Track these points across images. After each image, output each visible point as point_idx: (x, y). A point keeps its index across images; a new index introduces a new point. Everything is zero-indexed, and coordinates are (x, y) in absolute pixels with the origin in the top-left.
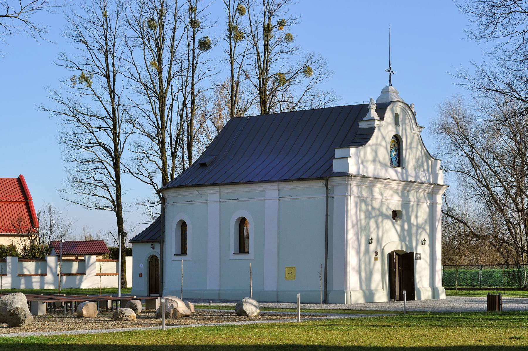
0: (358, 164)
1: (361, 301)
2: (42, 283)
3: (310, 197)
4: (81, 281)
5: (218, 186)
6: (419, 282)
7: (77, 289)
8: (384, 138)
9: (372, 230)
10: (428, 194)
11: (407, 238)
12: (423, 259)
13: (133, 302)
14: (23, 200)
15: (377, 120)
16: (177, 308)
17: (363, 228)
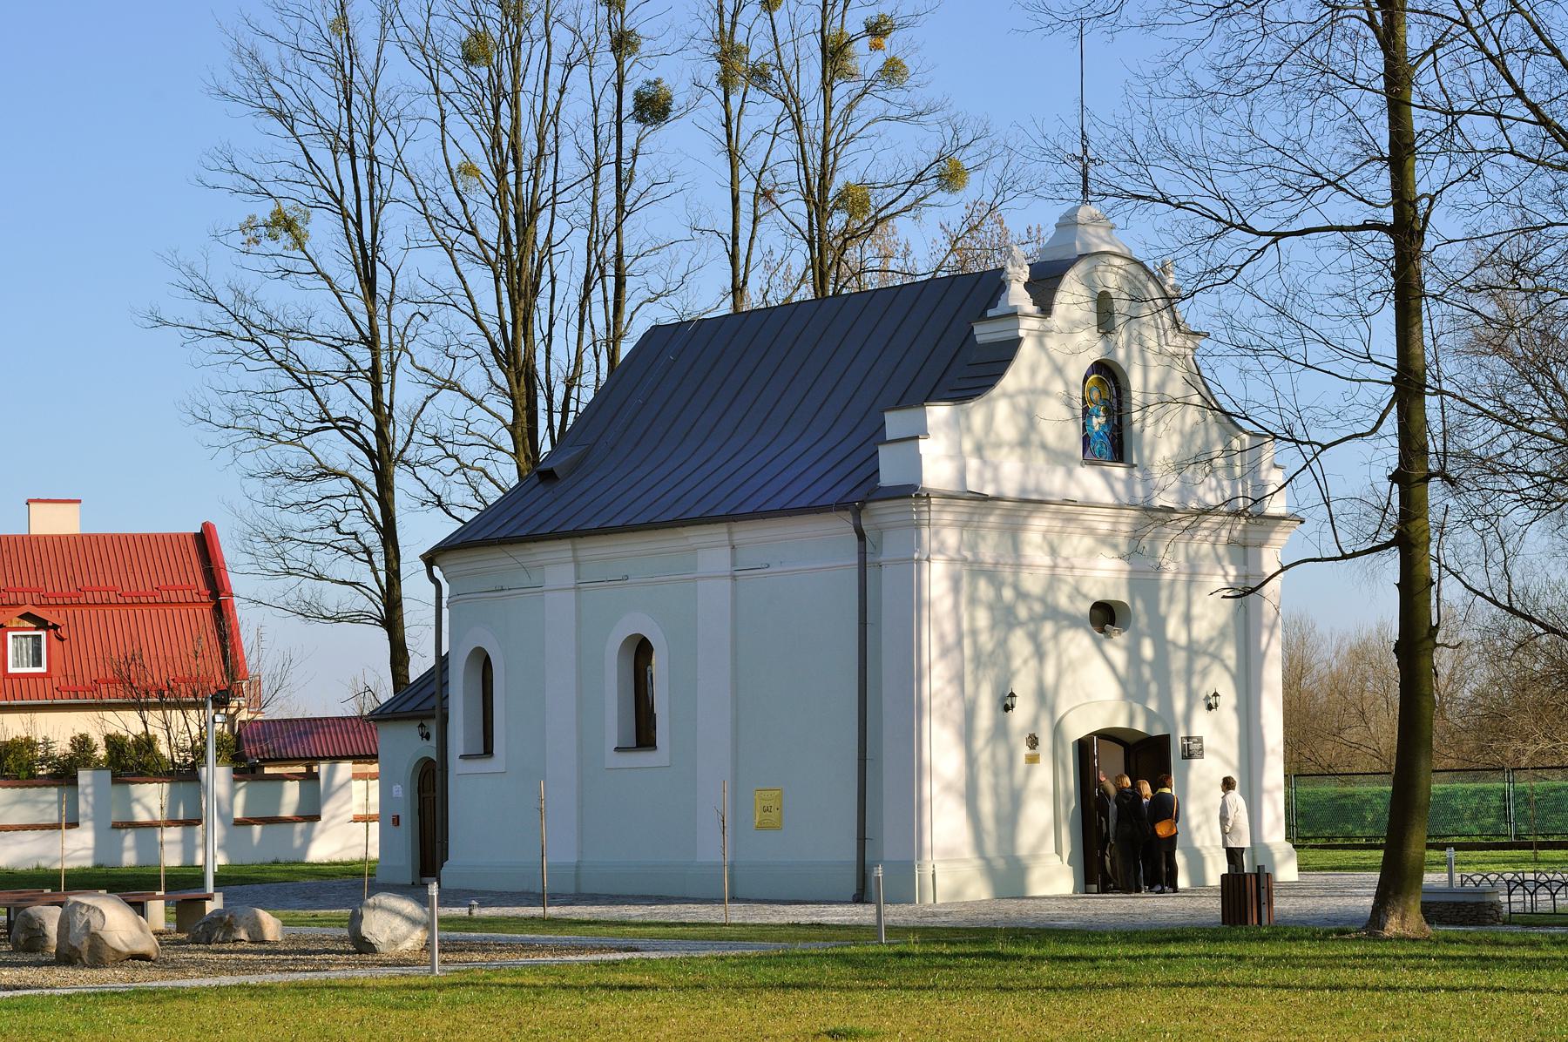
0: (959, 455)
1: (978, 891)
2: (188, 847)
3: (819, 566)
4: (308, 839)
5: (568, 541)
6: (1198, 828)
7: (295, 863)
8: (1059, 370)
9: (1017, 663)
10: (1230, 543)
11: (1153, 688)
12: (1216, 753)
13: (32, 914)
14: (204, 599)
15: (1027, 315)
16: (100, 933)
17: (984, 659)
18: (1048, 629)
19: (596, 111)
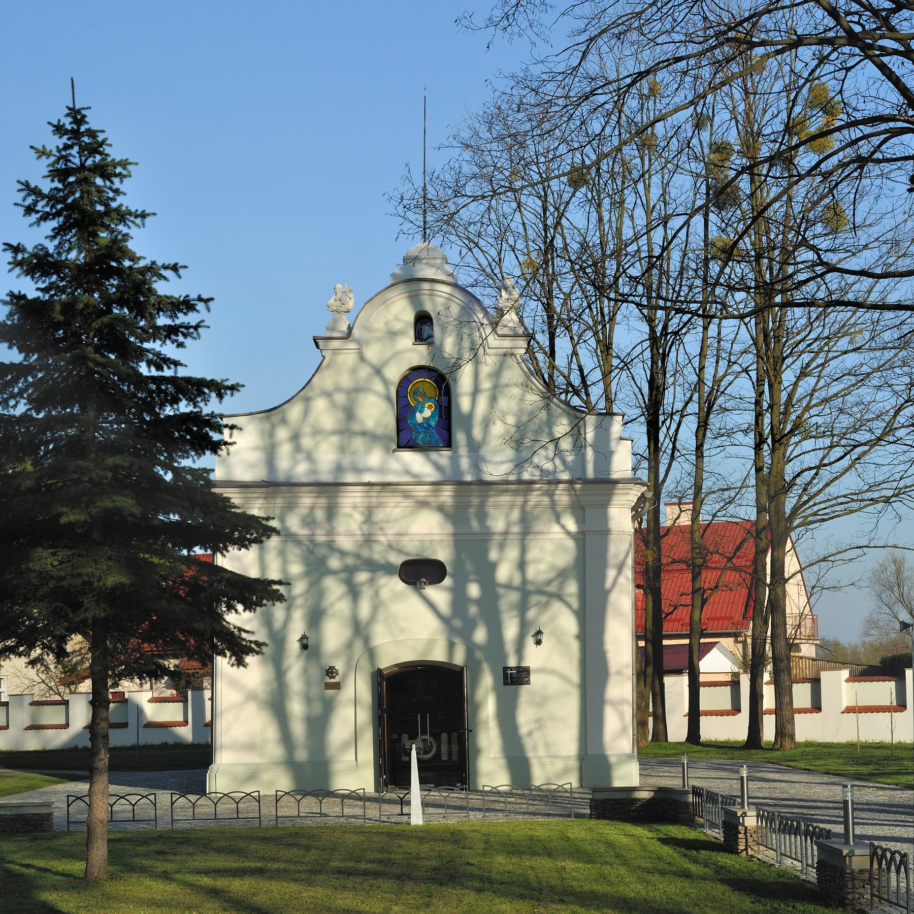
18: (362, 577)
19: (824, 559)
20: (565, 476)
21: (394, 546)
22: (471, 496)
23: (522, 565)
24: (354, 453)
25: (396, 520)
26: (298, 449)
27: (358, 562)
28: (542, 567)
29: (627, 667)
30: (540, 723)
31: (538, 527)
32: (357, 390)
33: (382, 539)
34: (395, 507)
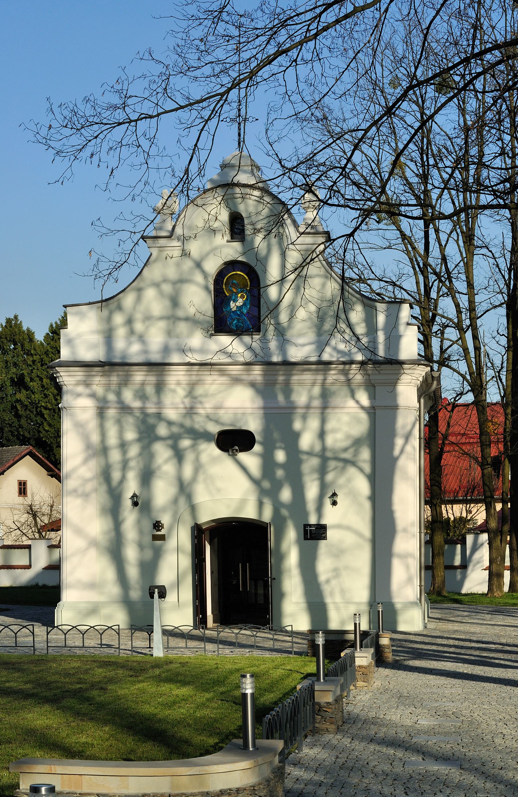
18: (186, 443)
20: (359, 357)
21: (212, 417)
22: (276, 375)
23: (322, 434)
24: (178, 337)
25: (213, 395)
26: (132, 332)
27: (182, 430)
28: (339, 436)
29: (412, 524)
30: (336, 572)
31: (335, 401)
32: (182, 281)
33: (201, 411)
34: (212, 384)
